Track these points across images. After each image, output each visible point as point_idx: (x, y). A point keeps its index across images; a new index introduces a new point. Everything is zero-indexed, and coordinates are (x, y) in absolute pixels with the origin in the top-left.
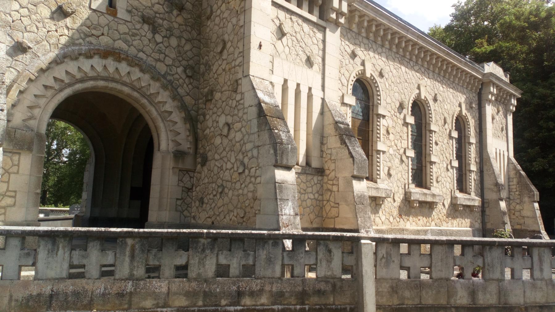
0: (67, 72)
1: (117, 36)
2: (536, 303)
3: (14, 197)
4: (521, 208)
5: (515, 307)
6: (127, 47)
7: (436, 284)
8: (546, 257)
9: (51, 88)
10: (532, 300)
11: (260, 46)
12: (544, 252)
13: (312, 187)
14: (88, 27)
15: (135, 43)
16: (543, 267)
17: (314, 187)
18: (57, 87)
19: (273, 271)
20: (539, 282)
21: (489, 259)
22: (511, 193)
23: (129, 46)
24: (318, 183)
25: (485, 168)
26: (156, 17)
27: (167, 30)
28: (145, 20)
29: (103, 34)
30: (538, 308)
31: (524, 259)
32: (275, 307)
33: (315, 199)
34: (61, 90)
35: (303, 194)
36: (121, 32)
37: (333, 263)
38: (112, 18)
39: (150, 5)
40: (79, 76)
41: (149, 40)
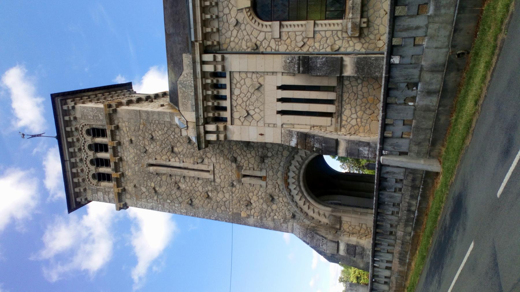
0: (300, 200)
2: (450, 35)
3: (362, 224)
5: (450, 57)
7: (417, 118)
9: (309, 206)
10: (446, 39)
11: (262, 135)
13: (352, 86)
15: (276, 167)
16: (415, 26)
17: (353, 84)
18: (308, 204)
19: (398, 196)
20: (430, 31)
21: (401, 79)
24: (349, 80)
30: (456, 34)
32: (419, 199)
33: (362, 83)
34: (309, 202)
35: (358, 97)
40: (300, 195)
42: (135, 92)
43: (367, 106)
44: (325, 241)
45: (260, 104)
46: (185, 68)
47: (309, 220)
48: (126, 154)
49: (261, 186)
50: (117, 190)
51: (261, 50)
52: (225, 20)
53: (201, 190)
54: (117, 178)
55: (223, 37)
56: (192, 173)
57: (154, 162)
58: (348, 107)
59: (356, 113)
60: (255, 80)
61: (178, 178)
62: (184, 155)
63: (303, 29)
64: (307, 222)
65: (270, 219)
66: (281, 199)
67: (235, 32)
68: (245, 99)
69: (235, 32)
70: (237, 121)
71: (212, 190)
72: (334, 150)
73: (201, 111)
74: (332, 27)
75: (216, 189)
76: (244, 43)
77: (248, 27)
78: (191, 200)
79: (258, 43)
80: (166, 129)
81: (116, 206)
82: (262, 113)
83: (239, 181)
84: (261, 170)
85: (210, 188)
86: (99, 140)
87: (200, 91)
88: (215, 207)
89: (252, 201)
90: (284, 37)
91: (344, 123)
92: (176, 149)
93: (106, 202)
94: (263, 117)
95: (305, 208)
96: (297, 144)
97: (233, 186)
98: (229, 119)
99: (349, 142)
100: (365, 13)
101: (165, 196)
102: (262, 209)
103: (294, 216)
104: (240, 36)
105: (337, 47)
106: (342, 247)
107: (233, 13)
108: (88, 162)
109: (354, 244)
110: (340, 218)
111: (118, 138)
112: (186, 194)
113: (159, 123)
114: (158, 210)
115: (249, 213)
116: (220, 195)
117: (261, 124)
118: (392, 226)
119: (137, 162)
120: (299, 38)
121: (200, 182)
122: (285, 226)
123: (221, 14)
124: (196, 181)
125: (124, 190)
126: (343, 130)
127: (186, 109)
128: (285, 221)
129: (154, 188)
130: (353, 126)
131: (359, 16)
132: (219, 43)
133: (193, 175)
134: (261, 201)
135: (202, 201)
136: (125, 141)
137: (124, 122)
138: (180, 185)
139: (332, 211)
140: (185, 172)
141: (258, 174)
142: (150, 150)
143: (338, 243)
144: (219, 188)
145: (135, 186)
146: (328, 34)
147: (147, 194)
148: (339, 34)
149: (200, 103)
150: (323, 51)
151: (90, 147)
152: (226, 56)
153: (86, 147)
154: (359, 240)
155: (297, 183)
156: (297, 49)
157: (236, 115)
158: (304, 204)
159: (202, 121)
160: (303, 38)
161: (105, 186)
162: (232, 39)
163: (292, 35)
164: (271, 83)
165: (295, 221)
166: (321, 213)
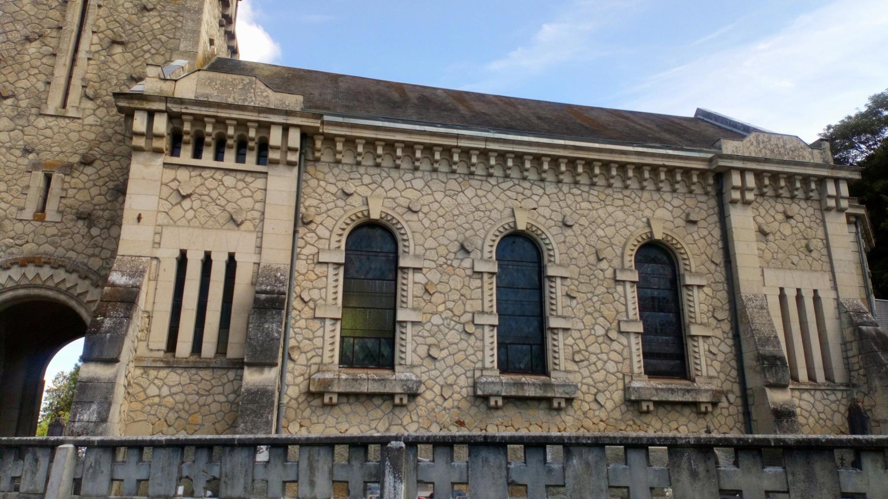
1: (43, 239)
4: (873, 403)
6: (54, 249)
8: (321, 462)
11: (139, 218)
12: (319, 454)
13: (223, 385)
14: (12, 238)
22: (853, 373)
23: (56, 248)
24: (235, 379)
25: (742, 328)
26: (94, 209)
27: (107, 220)
28: (80, 216)
29: (27, 242)
31: (284, 466)
35: (203, 395)
36: (49, 235)
37: (38, 475)
38: (40, 223)
39: (88, 198)
41: (83, 236)
43: (183, 414)
45: (203, 220)
46: (279, 96)
49: (22, 209)
51: (302, 230)
53: (19, 84)
55: (327, 170)
56: (61, 73)
59: (171, 395)
62: (104, 63)
68: (214, 194)
69: (333, 189)
70: (170, 174)
72: (96, 355)
75: (20, 115)
76: (315, 202)
77: (339, 212)
80: (164, 38)
82: (183, 222)
87: (235, 114)
90: (319, 270)
91: (153, 373)
92: (118, 49)
96: (113, 285)
97: (27, 151)
99: (111, 384)
100: (345, 400)
104: (327, 197)
105: (295, 356)
107: (363, 190)
117: (162, 219)
120: (315, 294)
121: (41, 86)
123: (362, 170)
124: (42, 77)
126: (139, 372)
127: (200, 83)
132: (317, 160)
133: (57, 73)
138: (36, 44)
144: (23, 122)
146: (318, 342)
148: (317, 360)
149: (212, 112)
150: (291, 333)
156: (298, 289)
157: (183, 174)
159: (176, 108)
162: (322, 183)
163: (321, 283)
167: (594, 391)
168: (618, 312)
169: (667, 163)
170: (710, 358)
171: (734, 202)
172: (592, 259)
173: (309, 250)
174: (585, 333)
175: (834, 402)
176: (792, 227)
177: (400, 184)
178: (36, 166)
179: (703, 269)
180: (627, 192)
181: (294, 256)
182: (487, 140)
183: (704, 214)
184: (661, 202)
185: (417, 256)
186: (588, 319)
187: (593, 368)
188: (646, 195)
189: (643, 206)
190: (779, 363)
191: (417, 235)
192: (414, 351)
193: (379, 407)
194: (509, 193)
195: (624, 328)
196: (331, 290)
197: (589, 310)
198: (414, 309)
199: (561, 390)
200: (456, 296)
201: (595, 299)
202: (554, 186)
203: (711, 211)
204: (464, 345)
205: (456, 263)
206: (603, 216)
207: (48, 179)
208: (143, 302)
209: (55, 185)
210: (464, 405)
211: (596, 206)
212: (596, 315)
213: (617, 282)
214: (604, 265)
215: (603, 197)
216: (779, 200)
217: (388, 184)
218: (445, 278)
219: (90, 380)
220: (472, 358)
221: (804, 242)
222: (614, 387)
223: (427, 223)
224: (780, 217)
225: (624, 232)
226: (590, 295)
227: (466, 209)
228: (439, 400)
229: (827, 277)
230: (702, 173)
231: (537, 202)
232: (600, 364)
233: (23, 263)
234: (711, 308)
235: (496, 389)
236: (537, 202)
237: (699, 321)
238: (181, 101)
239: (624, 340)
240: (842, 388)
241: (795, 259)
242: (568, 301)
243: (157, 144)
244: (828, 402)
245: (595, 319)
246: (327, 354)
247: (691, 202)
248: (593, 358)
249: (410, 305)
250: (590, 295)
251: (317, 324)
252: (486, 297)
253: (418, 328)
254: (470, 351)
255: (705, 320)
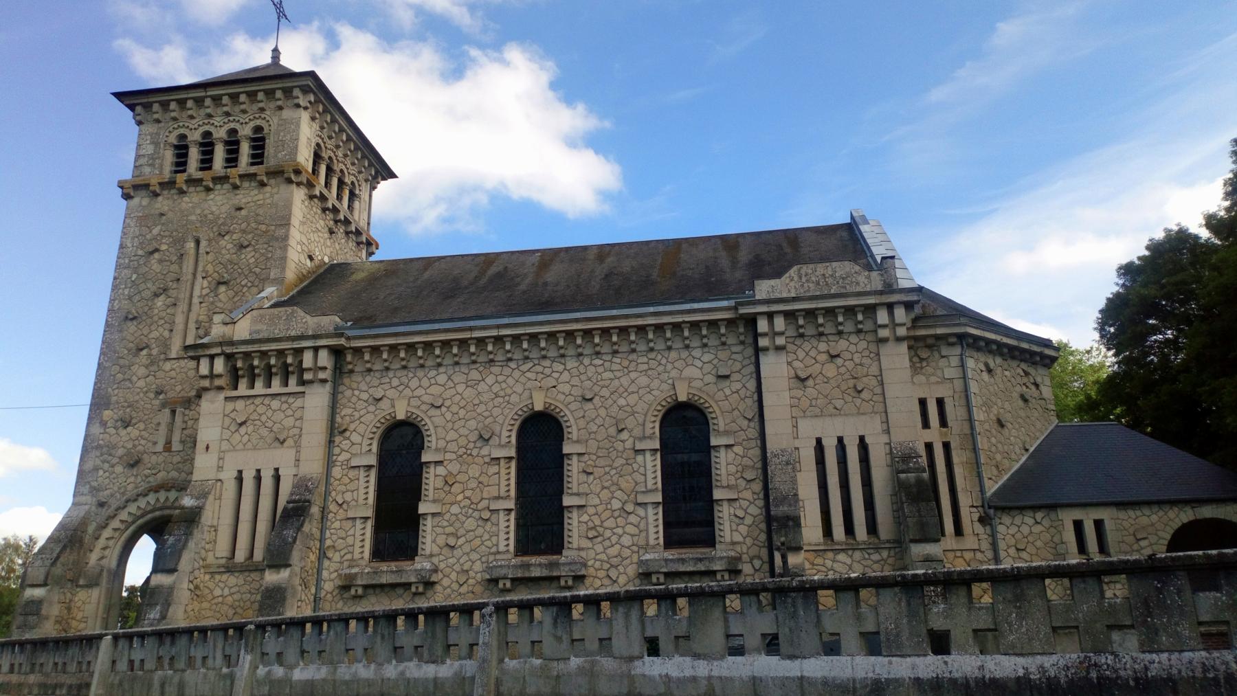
11: (207, 448)
40: (139, 513)
42: (375, 188)
43: (239, 610)
44: (48, 563)
45: (255, 442)
46: (316, 319)
47: (94, 531)
48: (218, 198)
49: (155, 443)
50: (154, 181)
51: (337, 439)
52: (383, 381)
53: (152, 336)
54: (175, 182)
55: (360, 379)
56: (180, 319)
57: (202, 250)
58: (241, 582)
59: (231, 594)
60: (291, 433)
61: (173, 293)
62: (212, 303)
63: (361, 501)
64: (91, 529)
65: (98, 462)
66: (132, 479)
67: (365, 396)
68: (264, 418)
69: (365, 396)
70: (230, 406)
71: (150, 355)
72: (160, 567)
73: (243, 349)
74: (503, 536)
75: (152, 363)
76: (349, 411)
77: (370, 417)
78: (135, 318)
79: (347, 434)
80: (257, 270)
81: (126, 181)
82: (241, 446)
83: (164, 405)
84: (182, 442)
85: (155, 352)
86: (245, 149)
87: (274, 346)
88: (122, 362)
89: (129, 429)
90: (352, 474)
91: (218, 577)
92: (222, 288)
93: (136, 161)
94: (234, 449)
95: (115, 523)
96: (183, 508)
97: (158, 393)
98: (235, 393)
99: (171, 589)
100: (371, 591)
101: (143, 270)
102: (114, 447)
103: (101, 505)
104: (361, 405)
105: (330, 554)
106: (38, 592)
107: (391, 393)
108: (207, 128)
109: (44, 612)
110: (97, 585)
111: (246, 184)
112: (146, 309)
113: (267, 258)
114: (118, 258)
115: (109, 424)
116: (142, 371)
117: (225, 446)
118: (42, 665)
119: (203, 219)
120: (348, 497)
121: (166, 334)
122: (86, 489)
123: (391, 374)
124: (167, 326)
125: (156, 195)
126: (207, 577)
127: (254, 321)
128: (94, 490)
129: (157, 250)
130: (211, 591)
131: (364, 582)
132: (352, 371)
133: (177, 321)
134: (130, 445)
135: (132, 339)
136: (241, 198)
137: (272, 196)
138: (162, 298)
139: (109, 571)
140: (182, 307)
141: (176, 437)
142: (223, 243)
143: (45, 585)
144: (154, 368)
145: (162, 215)
146: (350, 540)
147: (148, 237)
148: (349, 556)
149: (256, 347)
150: (328, 534)
151: (233, 132)
152: (328, 386)
153: (232, 125)
154: (52, 620)
155: (158, 505)
156: (333, 494)
157: (240, 405)
158: (122, 521)
159: (228, 350)
160: (348, 503)
161: (163, 158)
162: (356, 393)
163: (352, 486)
164: (283, 458)
165: (94, 508)
166: (107, 552)
167: (606, 566)
168: (637, 484)
169: (687, 319)
170: (736, 525)
171: (766, 349)
172: (613, 431)
173: (344, 457)
174: (600, 509)
175: (877, 562)
176: (838, 368)
177: (425, 382)
178: (164, 405)
179: (734, 427)
180: (652, 355)
181: (329, 463)
182: (498, 327)
183: (738, 366)
184: (690, 361)
185: (437, 450)
186: (605, 494)
187: (607, 543)
188: (673, 355)
189: (669, 366)
190: (791, 523)
191: (440, 430)
192: (434, 541)
193: (401, 596)
194: (528, 375)
195: (641, 499)
196: (362, 491)
197: (606, 484)
198: (434, 501)
199: (567, 568)
200: (473, 484)
201: (613, 472)
202: (575, 359)
203: (747, 362)
204: (480, 530)
205: (475, 452)
206: (626, 384)
207: (173, 412)
208: (207, 518)
209: (178, 418)
210: (478, 589)
211: (618, 374)
212: (613, 488)
213: (637, 452)
214: (625, 435)
215: (626, 363)
216: (824, 338)
217: (414, 383)
218: (464, 468)
219: (158, 587)
220: (488, 543)
221: (851, 383)
222: (628, 561)
223: (449, 416)
224: (824, 357)
225: (649, 398)
226: (607, 469)
227: (485, 397)
228: (455, 586)
229: (877, 420)
230: (730, 322)
231: (557, 379)
232: (614, 539)
233: (156, 489)
234: (740, 468)
235: (503, 572)
236: (557, 379)
237: (725, 483)
238: (232, 343)
239: (641, 512)
240: (887, 545)
241: (839, 403)
242: (583, 477)
243: (218, 382)
244: (870, 562)
245: (612, 493)
246: (357, 550)
247: (723, 355)
248: (608, 533)
249: (431, 497)
250: (607, 469)
251: (350, 523)
252: (506, 480)
253: (437, 519)
254: (486, 536)
255: (733, 482)
